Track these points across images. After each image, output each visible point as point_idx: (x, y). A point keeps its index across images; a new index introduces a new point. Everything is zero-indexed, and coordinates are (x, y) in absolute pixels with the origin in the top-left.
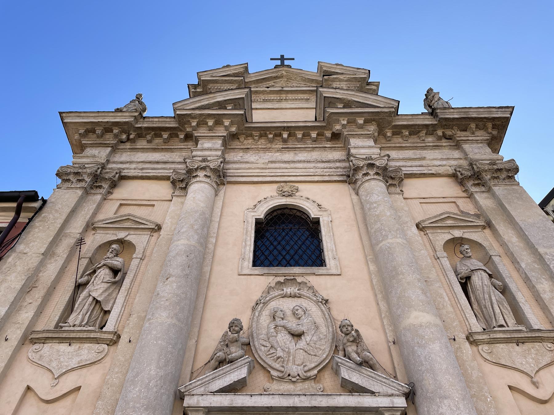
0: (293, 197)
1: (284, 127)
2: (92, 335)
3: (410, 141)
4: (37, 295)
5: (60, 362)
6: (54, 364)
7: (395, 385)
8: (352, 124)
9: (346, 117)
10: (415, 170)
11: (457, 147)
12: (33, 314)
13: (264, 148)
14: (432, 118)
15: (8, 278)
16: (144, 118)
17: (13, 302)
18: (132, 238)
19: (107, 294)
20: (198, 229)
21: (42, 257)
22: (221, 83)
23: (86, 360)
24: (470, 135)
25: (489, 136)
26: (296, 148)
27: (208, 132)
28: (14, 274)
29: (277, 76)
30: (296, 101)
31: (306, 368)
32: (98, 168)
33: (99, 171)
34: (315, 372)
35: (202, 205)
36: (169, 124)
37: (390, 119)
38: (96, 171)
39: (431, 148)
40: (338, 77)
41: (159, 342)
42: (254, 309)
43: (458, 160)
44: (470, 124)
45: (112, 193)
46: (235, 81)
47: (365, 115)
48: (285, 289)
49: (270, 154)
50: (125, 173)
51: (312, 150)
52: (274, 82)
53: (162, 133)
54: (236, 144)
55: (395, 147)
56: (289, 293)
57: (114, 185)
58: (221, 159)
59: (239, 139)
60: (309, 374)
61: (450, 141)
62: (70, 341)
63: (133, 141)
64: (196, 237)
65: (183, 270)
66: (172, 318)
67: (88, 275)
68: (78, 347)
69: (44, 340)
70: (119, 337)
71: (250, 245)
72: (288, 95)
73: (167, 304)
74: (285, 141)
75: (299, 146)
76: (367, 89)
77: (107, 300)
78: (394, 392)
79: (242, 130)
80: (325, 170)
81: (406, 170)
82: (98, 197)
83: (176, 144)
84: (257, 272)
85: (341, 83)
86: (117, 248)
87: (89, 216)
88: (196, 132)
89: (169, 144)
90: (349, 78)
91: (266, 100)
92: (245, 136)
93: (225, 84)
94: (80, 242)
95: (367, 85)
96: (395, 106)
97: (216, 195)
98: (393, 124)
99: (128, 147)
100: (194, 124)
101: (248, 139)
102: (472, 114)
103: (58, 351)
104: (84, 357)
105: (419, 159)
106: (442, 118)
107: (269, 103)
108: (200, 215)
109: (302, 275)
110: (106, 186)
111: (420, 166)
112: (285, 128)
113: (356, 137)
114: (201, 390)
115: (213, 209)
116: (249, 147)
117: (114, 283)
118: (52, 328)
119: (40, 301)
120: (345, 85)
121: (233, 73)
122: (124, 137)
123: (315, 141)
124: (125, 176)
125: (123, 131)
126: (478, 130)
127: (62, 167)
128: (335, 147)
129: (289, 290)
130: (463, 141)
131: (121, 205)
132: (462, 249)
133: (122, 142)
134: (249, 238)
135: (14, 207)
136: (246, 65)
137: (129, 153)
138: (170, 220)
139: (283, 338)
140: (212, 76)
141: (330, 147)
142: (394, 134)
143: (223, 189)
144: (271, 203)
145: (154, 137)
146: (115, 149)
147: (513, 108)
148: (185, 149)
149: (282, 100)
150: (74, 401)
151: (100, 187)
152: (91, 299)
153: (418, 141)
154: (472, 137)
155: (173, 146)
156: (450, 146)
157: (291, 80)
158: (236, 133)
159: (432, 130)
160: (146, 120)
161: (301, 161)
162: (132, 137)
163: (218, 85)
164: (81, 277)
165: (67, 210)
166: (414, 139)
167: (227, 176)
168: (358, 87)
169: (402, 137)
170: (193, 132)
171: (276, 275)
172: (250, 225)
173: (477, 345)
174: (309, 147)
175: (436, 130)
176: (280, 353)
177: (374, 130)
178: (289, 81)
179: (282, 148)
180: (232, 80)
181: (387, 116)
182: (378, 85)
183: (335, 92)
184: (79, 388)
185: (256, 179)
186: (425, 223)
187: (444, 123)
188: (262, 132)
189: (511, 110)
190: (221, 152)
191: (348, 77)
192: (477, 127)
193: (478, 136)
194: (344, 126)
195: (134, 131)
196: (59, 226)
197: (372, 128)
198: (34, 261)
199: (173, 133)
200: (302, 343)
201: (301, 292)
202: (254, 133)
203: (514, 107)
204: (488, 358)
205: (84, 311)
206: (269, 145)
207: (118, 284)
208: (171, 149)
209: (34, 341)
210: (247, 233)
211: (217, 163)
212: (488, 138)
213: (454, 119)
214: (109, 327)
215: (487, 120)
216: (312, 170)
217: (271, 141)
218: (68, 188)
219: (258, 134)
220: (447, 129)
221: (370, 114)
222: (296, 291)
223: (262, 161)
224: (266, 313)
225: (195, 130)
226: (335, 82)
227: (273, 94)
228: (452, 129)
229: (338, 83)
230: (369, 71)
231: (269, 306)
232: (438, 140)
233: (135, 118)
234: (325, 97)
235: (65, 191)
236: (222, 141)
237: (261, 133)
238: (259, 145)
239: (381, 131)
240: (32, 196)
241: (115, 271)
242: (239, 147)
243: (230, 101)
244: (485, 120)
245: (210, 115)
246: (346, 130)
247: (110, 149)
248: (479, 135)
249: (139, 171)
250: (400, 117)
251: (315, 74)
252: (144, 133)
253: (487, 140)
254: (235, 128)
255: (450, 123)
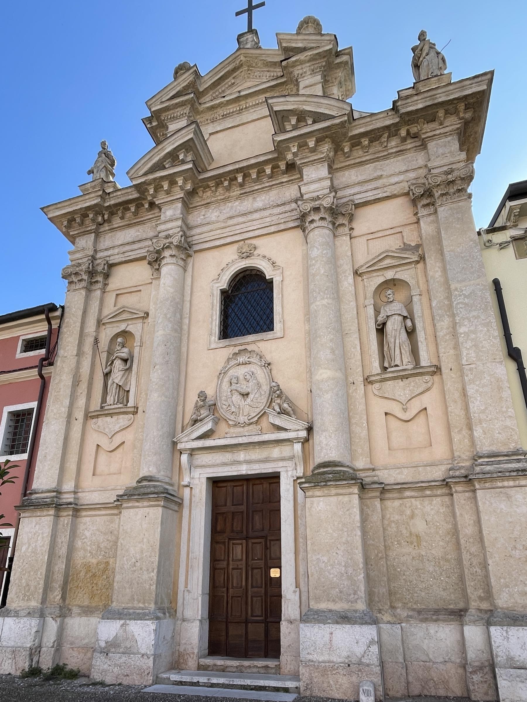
0: (252, 257)
1: (237, 169)
2: (122, 410)
3: (371, 151)
4: (83, 387)
5: (110, 429)
6: (107, 430)
7: (300, 424)
8: (304, 148)
9: (295, 141)
10: (370, 196)
11: (424, 147)
12: (85, 400)
13: (223, 199)
14: (394, 115)
15: (62, 378)
16: (109, 193)
17: (71, 395)
18: (130, 328)
19: (124, 378)
20: (170, 318)
21: (76, 358)
22: (173, 109)
23: (123, 426)
24: (438, 128)
25: (460, 123)
26: (253, 191)
27: (167, 196)
28: (65, 375)
29: (235, 68)
30: (258, 107)
31: (249, 418)
32: (89, 264)
33: (91, 267)
34: (256, 419)
35: (172, 290)
36: (131, 195)
37: (344, 130)
38: (89, 268)
39: (393, 155)
40: (298, 58)
41: (156, 414)
42: (218, 378)
43: (418, 169)
44: (437, 112)
45: (108, 284)
46: (186, 101)
47: (315, 134)
48: (239, 359)
49: (230, 204)
50: (113, 260)
51: (270, 189)
52: (234, 78)
53: (130, 206)
54: (197, 201)
55: (354, 164)
56: (241, 362)
57: (107, 276)
58: (181, 233)
59: (197, 193)
60: (251, 421)
61: (416, 139)
62: (111, 415)
63: (109, 221)
64: (170, 325)
65: (164, 358)
66: (161, 397)
67: (110, 365)
68: (116, 418)
69: (97, 416)
70: (137, 408)
71: (216, 319)
72: (247, 101)
73: (157, 387)
74: (242, 185)
75: (256, 188)
76: (337, 63)
77: (126, 383)
78: (299, 428)
79: (198, 184)
80: (281, 216)
81: (358, 199)
82: (98, 292)
83: (145, 215)
84: (221, 345)
85: (304, 66)
86: (121, 341)
87: (96, 314)
88: (156, 199)
89: (139, 216)
90: (312, 56)
91: (226, 115)
92: (202, 189)
93: (177, 108)
94: (96, 341)
95: (337, 56)
96: (347, 112)
97: (185, 270)
98: (350, 134)
99: (107, 228)
100: (152, 191)
101: (207, 192)
102: (440, 97)
103: (107, 422)
104: (122, 424)
105: (375, 178)
106: (403, 113)
107: (228, 118)
108: (171, 302)
109: (254, 342)
110: (100, 278)
111: (376, 189)
112: (238, 171)
113: (309, 165)
114: (186, 439)
115: (184, 287)
116: (208, 201)
117: (127, 370)
118: (99, 409)
119: (86, 390)
120: (308, 68)
121: (183, 87)
122: (100, 219)
123: (271, 178)
124: (113, 263)
125: (97, 214)
126: (449, 115)
127: (63, 269)
128: (292, 180)
129: (241, 359)
130: (429, 139)
131: (117, 295)
132: (387, 294)
133: (100, 225)
134: (214, 312)
135: (30, 383)
136: (195, 68)
137: (110, 234)
138: (154, 306)
139: (236, 398)
140: (162, 102)
141: (287, 182)
142: (353, 146)
143: (190, 261)
144: (232, 269)
145: (124, 211)
146: (98, 234)
147: (492, 73)
148: (153, 218)
149: (242, 109)
150: (123, 449)
151: (97, 282)
152: (115, 385)
153: (380, 149)
154: (440, 129)
155: (142, 217)
156: (416, 147)
157: (252, 67)
158: (193, 189)
159: (395, 131)
160: (111, 196)
161: (257, 210)
162: (106, 217)
163: (171, 112)
164: (106, 368)
165: (80, 313)
166: (376, 147)
167: (192, 245)
168: (324, 67)
169: (362, 148)
170: (154, 199)
171: (235, 346)
172: (215, 298)
173: (372, 384)
174: (266, 187)
175: (399, 130)
176: (233, 409)
177: (328, 150)
178: (251, 70)
179: (241, 194)
180: (182, 101)
181: (340, 128)
182: (350, 52)
183: (285, 102)
184: (124, 442)
185: (218, 243)
186: (362, 269)
187: (407, 119)
188: (217, 180)
189: (489, 76)
190: (181, 221)
191: (310, 55)
192: (447, 112)
193: (447, 126)
194: (295, 154)
195: (106, 210)
196: (79, 329)
197: (326, 148)
198: (72, 362)
199: (138, 202)
200: (249, 400)
201: (251, 360)
202: (209, 183)
203: (494, 71)
204: (377, 393)
205: (114, 394)
206: (227, 194)
207: (130, 369)
208: (142, 221)
209: (92, 417)
210: (213, 307)
211: (177, 237)
212: (459, 126)
213: (417, 110)
214: (131, 404)
215: (458, 101)
216: (268, 219)
217: (228, 189)
218: (75, 290)
219: (213, 184)
220: (412, 124)
221: (321, 131)
222: (247, 359)
223: (222, 217)
224: (226, 380)
225: (155, 198)
226: (296, 66)
227: (231, 104)
228: (417, 123)
229: (299, 67)
230: (335, 36)
231: (228, 374)
232: (402, 142)
233: (101, 197)
234: (276, 112)
235: (73, 293)
236: (182, 204)
237: (216, 182)
238: (218, 196)
239: (337, 148)
240: (52, 308)
241: (125, 361)
242: (200, 204)
243: (180, 147)
244: (455, 102)
245: (162, 178)
246: (298, 158)
247: (93, 235)
248: (448, 125)
249: (122, 256)
250: (357, 123)
251: (277, 52)
252: (115, 210)
253: (458, 129)
254: (190, 185)
255: (414, 116)
